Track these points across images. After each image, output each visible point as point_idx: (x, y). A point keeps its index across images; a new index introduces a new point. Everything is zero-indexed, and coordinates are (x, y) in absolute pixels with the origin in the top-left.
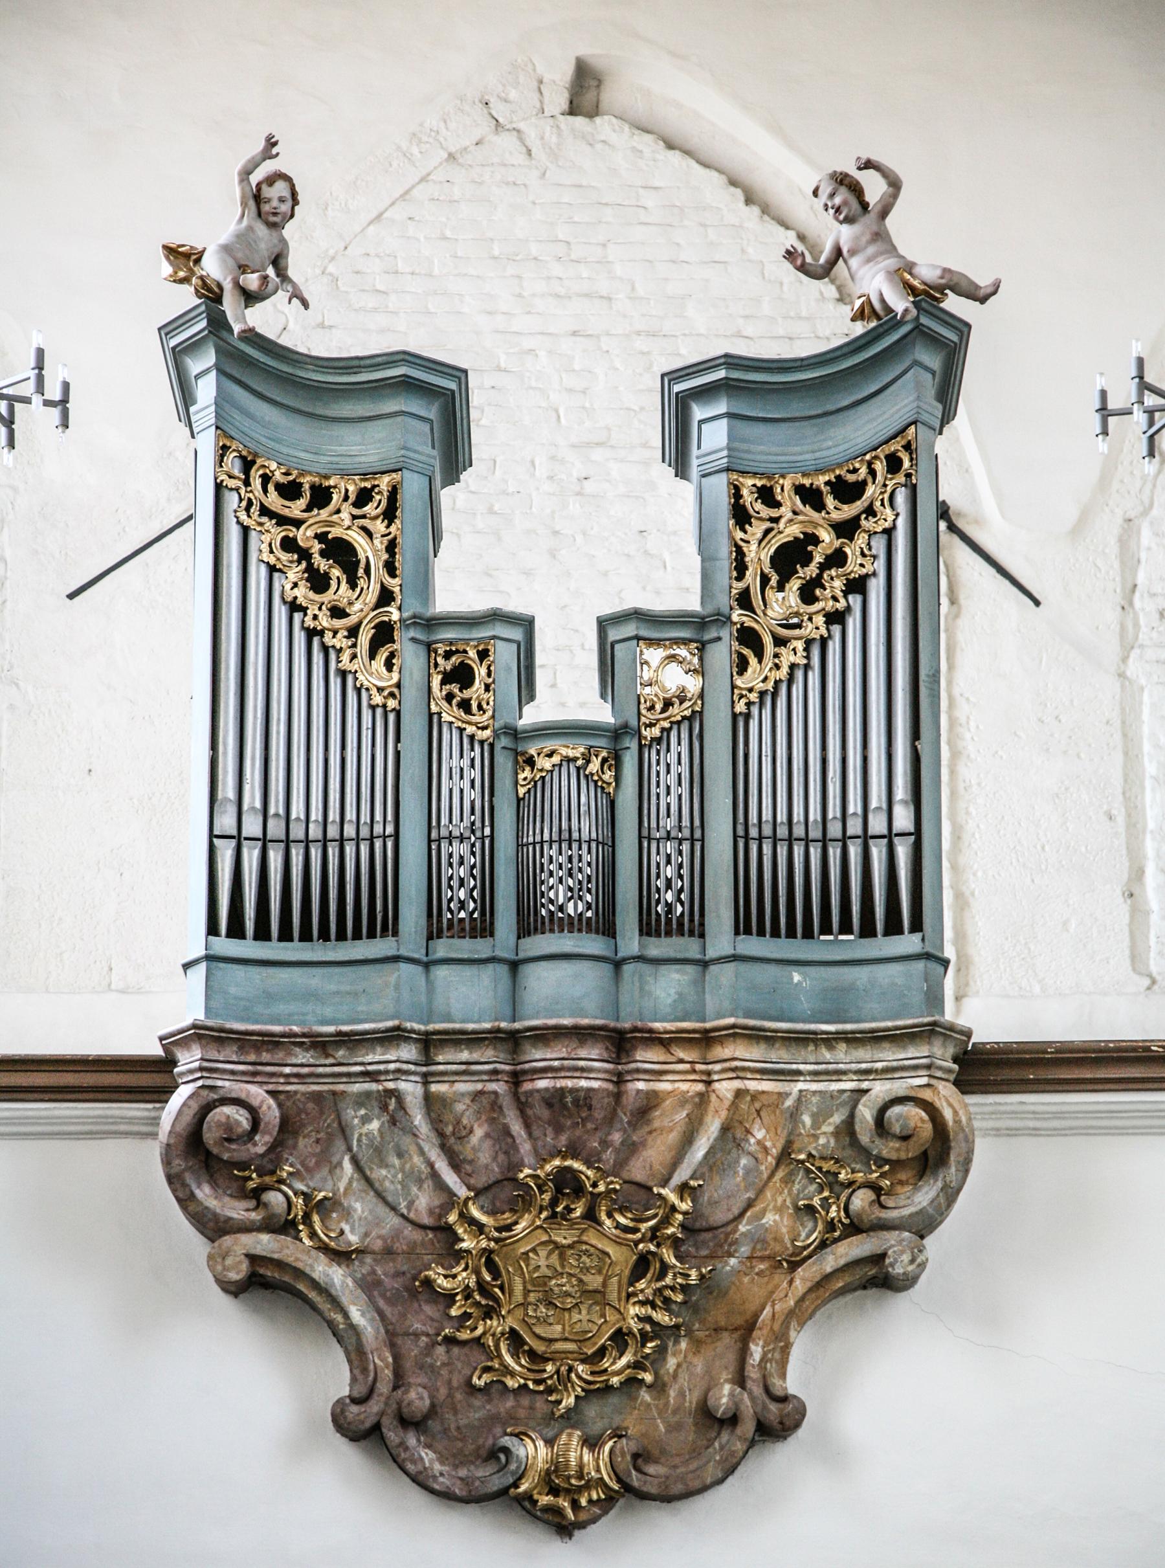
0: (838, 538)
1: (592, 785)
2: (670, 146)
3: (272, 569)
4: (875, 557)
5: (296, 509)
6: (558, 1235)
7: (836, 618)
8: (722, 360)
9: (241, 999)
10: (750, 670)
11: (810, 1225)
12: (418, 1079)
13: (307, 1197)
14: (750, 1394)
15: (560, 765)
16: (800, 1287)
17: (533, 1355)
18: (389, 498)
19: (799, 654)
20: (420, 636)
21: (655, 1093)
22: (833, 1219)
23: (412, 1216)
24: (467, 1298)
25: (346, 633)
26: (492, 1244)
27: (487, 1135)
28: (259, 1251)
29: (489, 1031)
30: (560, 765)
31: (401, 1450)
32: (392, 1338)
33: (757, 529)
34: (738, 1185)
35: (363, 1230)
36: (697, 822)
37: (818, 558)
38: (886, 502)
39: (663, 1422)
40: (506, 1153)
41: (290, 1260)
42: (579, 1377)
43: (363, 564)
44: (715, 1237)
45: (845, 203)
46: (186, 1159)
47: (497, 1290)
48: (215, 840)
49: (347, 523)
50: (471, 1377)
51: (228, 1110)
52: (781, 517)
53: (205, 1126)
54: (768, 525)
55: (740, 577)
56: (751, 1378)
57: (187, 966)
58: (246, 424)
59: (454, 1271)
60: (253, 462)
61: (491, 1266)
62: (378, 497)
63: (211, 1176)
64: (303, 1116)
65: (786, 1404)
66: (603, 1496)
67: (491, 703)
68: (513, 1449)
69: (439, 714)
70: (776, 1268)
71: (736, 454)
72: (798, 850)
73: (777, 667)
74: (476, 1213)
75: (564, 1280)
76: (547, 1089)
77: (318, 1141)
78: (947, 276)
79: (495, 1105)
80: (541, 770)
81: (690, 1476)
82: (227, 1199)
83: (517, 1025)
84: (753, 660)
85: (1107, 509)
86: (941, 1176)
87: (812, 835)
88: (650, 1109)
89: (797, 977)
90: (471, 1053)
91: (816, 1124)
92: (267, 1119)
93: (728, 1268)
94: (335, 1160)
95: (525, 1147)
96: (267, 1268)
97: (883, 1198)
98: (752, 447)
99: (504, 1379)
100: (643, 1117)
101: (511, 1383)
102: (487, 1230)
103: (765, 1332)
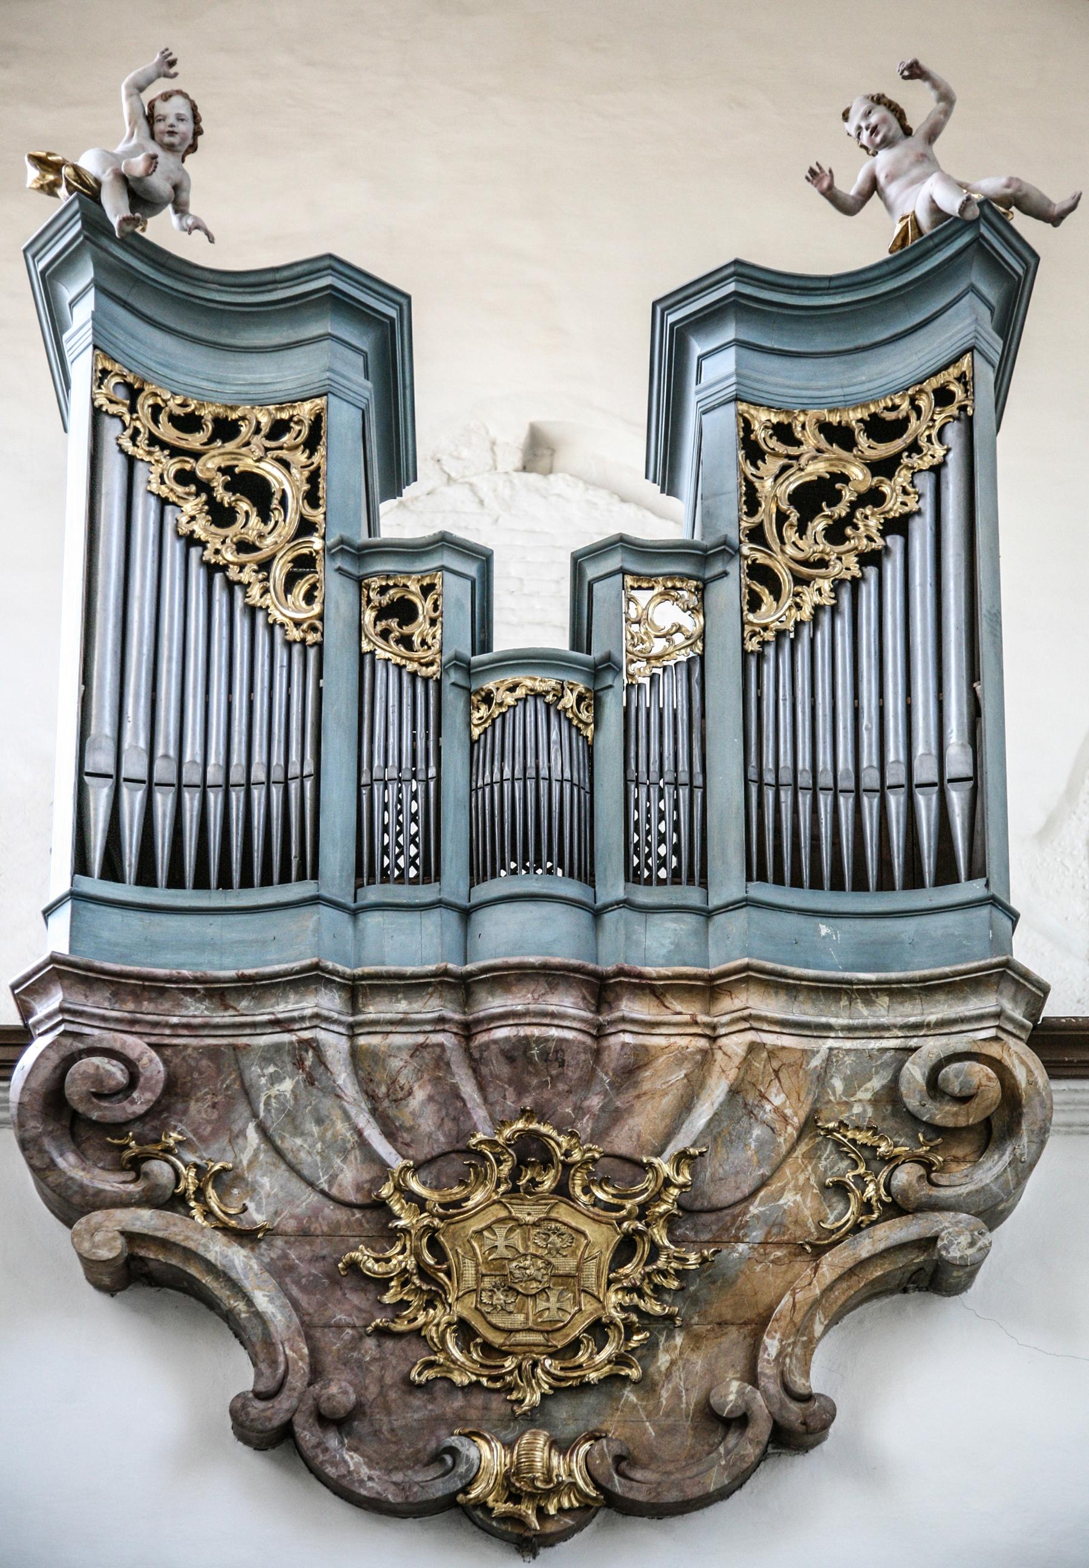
0: (873, 476)
1: (565, 725)
2: (623, 500)
3: (164, 502)
4: (920, 496)
5: (195, 441)
6: (521, 1212)
7: (872, 559)
8: (731, 270)
9: (116, 945)
10: (764, 608)
11: (840, 1207)
12: (342, 1030)
13: (200, 1170)
14: (765, 1393)
15: (525, 700)
16: (827, 1273)
17: (487, 1348)
18: (311, 428)
19: (825, 595)
20: (348, 567)
21: (645, 1048)
22: (869, 1200)
23: (334, 1192)
24: (403, 1285)
25: (256, 567)
26: (436, 1222)
27: (430, 1098)
28: (137, 1227)
29: (434, 975)
30: (525, 700)
31: (319, 1451)
32: (308, 1330)
33: (772, 465)
34: (749, 1160)
35: (272, 1209)
36: (697, 768)
37: (848, 495)
38: (934, 439)
39: (653, 1425)
40: (455, 1119)
41: (179, 1239)
42: (547, 1373)
43: (278, 496)
44: (718, 1220)
45: (884, 121)
46: (44, 1122)
47: (441, 1275)
48: (86, 778)
49: (259, 453)
50: (409, 1373)
51: (96, 1060)
52: (801, 455)
53: (68, 1078)
54: (786, 461)
55: (752, 511)
56: (765, 1375)
57: (48, 912)
58: (132, 347)
59: (388, 1254)
60: (141, 390)
61: (435, 1246)
62: (297, 428)
63: (78, 1146)
64: (196, 1075)
65: (811, 1404)
66: (576, 1504)
67: (438, 636)
68: (461, 1449)
69: (372, 653)
70: (796, 1255)
71: (747, 382)
72: (825, 801)
73: (799, 607)
74: (415, 1185)
75: (528, 1263)
76: (507, 1039)
77: (214, 1106)
78: (1015, 185)
79: (441, 1061)
80: (501, 705)
81: (688, 1481)
82: (97, 1171)
83: (470, 967)
84: (767, 598)
85: (1074, 817)
86: (1009, 1149)
87: (841, 785)
88: (639, 1068)
89: (824, 930)
90: (410, 1003)
91: (849, 1090)
92: (148, 1074)
93: (736, 1255)
94: (236, 1128)
95: (479, 1114)
96: (149, 1249)
97: (933, 1175)
98: (767, 378)
99: (449, 1375)
100: (628, 1078)
101: (458, 1378)
102: (429, 1205)
103: (783, 1323)
